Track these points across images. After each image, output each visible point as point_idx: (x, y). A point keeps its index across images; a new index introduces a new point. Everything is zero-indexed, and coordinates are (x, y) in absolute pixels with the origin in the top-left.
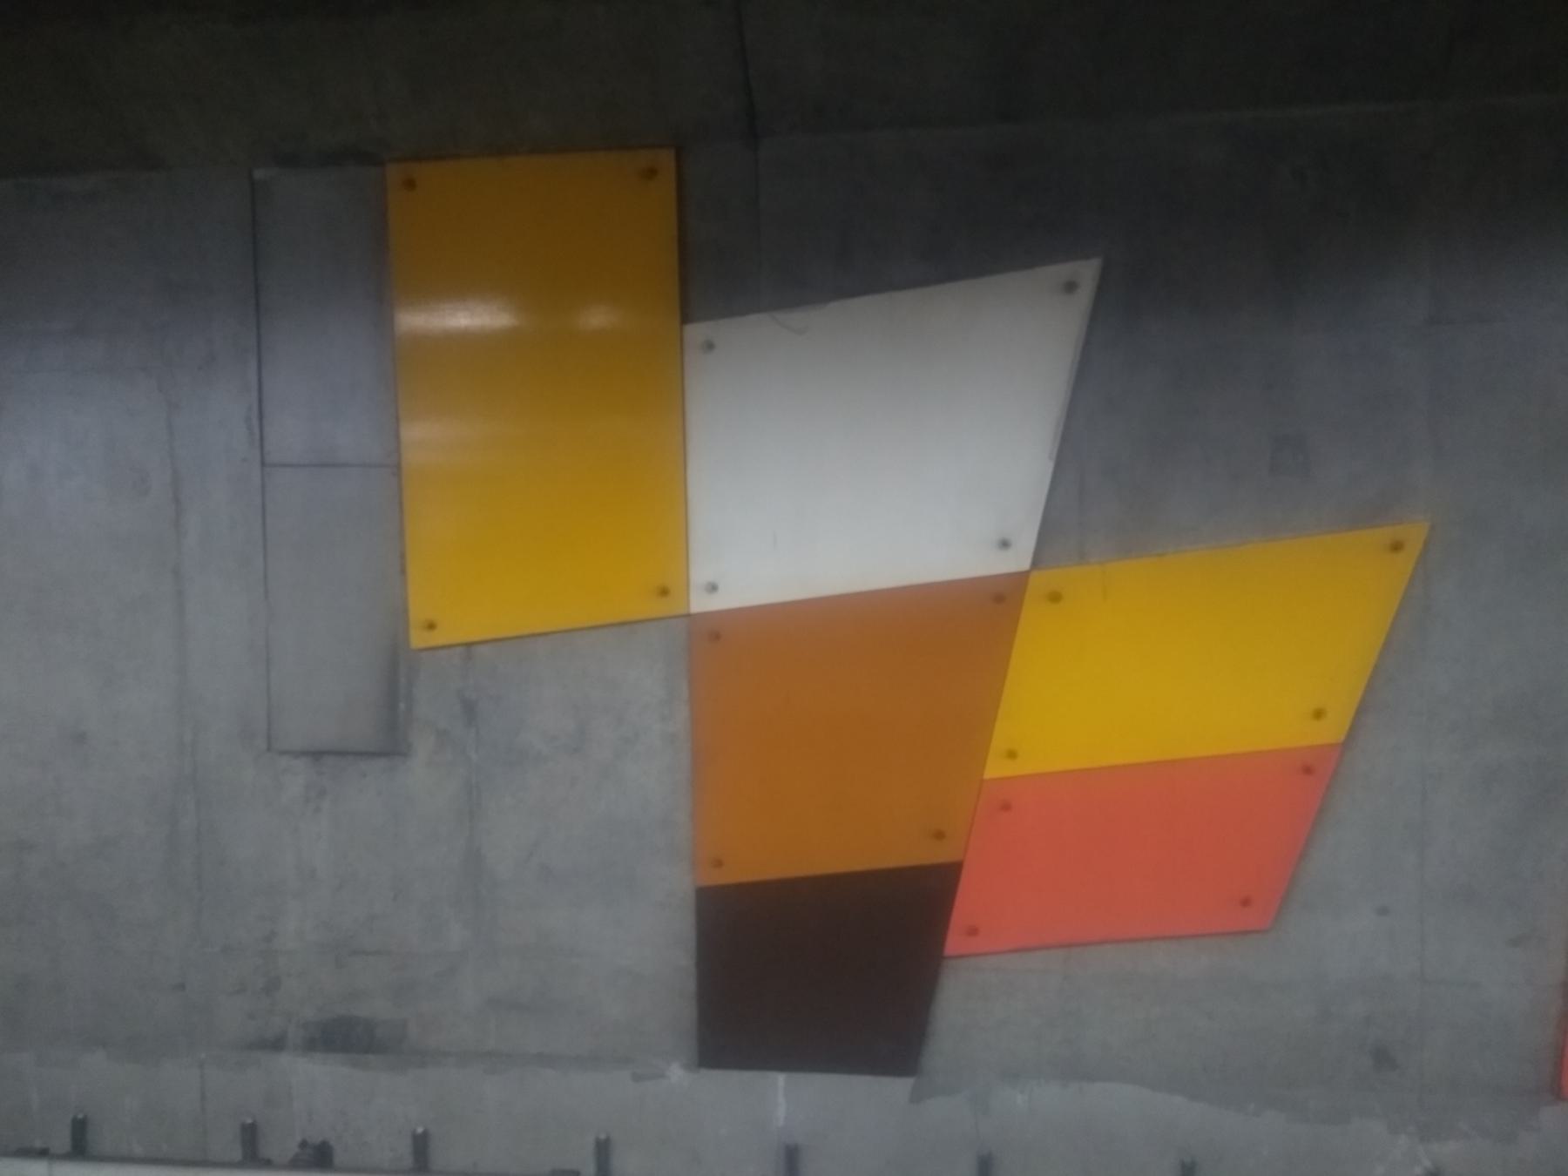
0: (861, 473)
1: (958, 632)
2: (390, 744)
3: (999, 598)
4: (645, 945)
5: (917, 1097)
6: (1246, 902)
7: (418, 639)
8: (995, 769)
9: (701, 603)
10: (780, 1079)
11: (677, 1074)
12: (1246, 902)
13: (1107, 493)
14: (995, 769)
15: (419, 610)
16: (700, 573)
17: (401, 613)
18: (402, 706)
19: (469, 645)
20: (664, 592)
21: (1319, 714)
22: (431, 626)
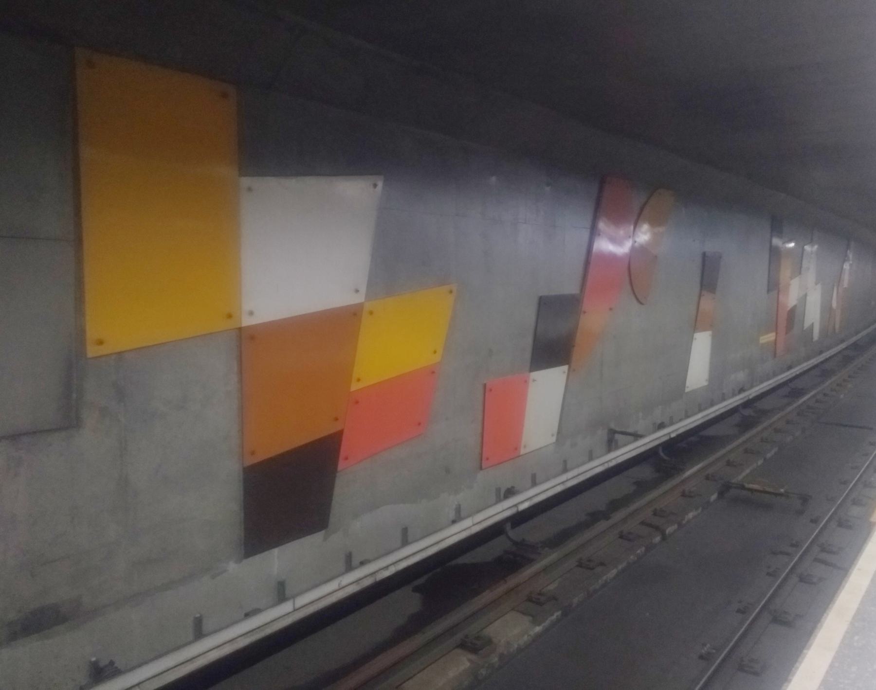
0: (301, 254)
1: (336, 328)
2: (69, 420)
3: (355, 314)
4: (218, 502)
5: (325, 539)
6: (336, 419)
7: (92, 351)
8: (355, 387)
9: (247, 321)
10: (276, 551)
11: (232, 567)
12: (336, 419)
13: (396, 265)
14: (355, 387)
15: (92, 332)
16: (246, 306)
17: (80, 335)
18: (74, 396)
19: (120, 353)
20: (230, 316)
21: (435, 352)
22: (100, 342)
